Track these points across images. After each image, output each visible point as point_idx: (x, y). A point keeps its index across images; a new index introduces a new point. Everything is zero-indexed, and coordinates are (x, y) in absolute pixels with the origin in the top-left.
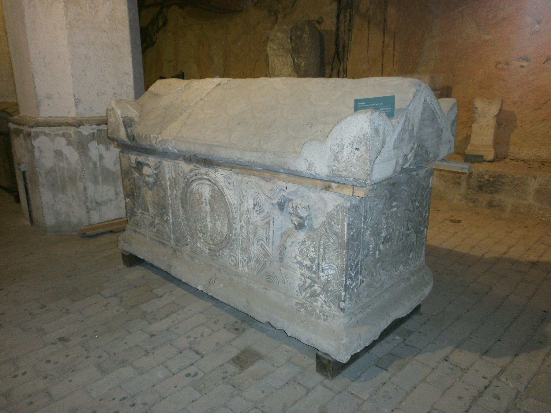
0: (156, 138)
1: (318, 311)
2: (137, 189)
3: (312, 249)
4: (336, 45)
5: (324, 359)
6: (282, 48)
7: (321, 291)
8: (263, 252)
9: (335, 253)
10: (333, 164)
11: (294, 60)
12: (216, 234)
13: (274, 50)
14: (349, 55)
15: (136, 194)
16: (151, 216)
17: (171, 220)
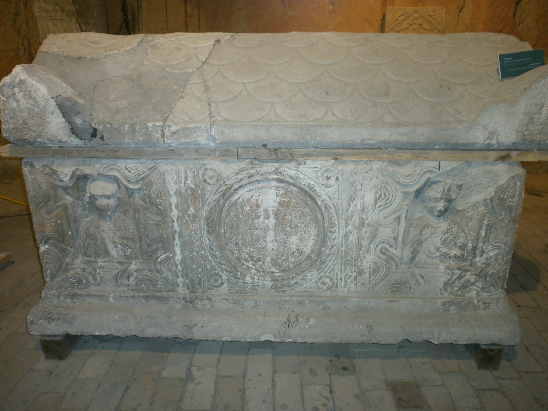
1: (476, 302)
2: (73, 223)
5: (492, 350)
6: (60, 9)
7: (475, 278)
8: (384, 257)
9: (505, 229)
12: (287, 255)
13: (47, 11)
14: (140, 24)
17: (179, 257)
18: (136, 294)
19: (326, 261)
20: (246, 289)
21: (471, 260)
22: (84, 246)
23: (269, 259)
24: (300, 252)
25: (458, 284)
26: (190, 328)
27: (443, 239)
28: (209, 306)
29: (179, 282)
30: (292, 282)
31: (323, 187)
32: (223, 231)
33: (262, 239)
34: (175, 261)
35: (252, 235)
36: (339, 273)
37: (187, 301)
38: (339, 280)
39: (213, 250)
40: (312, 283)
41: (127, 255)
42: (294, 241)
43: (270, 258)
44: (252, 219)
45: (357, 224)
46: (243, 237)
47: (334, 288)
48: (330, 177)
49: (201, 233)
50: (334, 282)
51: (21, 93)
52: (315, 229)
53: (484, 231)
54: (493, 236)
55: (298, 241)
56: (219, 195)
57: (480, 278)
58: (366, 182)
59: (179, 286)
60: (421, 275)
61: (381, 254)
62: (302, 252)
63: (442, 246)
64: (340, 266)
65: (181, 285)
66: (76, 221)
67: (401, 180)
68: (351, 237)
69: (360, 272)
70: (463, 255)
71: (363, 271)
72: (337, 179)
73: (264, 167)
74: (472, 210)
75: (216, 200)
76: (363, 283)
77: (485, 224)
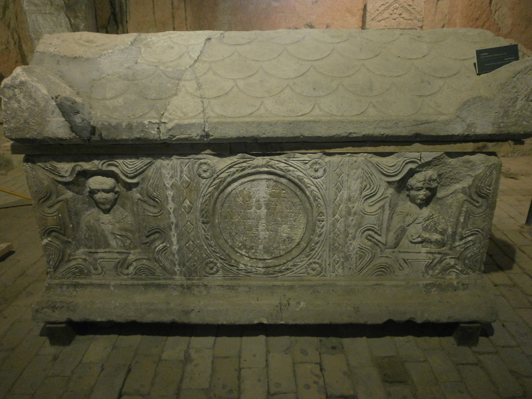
0: (157, 126)
3: (442, 221)
7: (455, 261)
11: (70, 20)
12: (278, 243)
17: (175, 247)
18: (136, 282)
20: (240, 275)
21: (451, 244)
22: (85, 238)
23: (261, 247)
25: (439, 267)
26: (187, 313)
27: (425, 225)
28: (205, 292)
30: (283, 268)
31: (311, 178)
33: (254, 228)
34: (171, 250)
36: (327, 259)
38: (327, 266)
40: (302, 269)
43: (262, 245)
47: (323, 273)
49: (196, 223)
50: (323, 267)
54: (471, 222)
56: (212, 188)
58: (352, 173)
61: (366, 241)
63: (423, 232)
64: (328, 252)
65: (178, 272)
67: (386, 170)
68: (338, 225)
69: (347, 258)
71: (350, 256)
72: (325, 171)
76: (350, 268)
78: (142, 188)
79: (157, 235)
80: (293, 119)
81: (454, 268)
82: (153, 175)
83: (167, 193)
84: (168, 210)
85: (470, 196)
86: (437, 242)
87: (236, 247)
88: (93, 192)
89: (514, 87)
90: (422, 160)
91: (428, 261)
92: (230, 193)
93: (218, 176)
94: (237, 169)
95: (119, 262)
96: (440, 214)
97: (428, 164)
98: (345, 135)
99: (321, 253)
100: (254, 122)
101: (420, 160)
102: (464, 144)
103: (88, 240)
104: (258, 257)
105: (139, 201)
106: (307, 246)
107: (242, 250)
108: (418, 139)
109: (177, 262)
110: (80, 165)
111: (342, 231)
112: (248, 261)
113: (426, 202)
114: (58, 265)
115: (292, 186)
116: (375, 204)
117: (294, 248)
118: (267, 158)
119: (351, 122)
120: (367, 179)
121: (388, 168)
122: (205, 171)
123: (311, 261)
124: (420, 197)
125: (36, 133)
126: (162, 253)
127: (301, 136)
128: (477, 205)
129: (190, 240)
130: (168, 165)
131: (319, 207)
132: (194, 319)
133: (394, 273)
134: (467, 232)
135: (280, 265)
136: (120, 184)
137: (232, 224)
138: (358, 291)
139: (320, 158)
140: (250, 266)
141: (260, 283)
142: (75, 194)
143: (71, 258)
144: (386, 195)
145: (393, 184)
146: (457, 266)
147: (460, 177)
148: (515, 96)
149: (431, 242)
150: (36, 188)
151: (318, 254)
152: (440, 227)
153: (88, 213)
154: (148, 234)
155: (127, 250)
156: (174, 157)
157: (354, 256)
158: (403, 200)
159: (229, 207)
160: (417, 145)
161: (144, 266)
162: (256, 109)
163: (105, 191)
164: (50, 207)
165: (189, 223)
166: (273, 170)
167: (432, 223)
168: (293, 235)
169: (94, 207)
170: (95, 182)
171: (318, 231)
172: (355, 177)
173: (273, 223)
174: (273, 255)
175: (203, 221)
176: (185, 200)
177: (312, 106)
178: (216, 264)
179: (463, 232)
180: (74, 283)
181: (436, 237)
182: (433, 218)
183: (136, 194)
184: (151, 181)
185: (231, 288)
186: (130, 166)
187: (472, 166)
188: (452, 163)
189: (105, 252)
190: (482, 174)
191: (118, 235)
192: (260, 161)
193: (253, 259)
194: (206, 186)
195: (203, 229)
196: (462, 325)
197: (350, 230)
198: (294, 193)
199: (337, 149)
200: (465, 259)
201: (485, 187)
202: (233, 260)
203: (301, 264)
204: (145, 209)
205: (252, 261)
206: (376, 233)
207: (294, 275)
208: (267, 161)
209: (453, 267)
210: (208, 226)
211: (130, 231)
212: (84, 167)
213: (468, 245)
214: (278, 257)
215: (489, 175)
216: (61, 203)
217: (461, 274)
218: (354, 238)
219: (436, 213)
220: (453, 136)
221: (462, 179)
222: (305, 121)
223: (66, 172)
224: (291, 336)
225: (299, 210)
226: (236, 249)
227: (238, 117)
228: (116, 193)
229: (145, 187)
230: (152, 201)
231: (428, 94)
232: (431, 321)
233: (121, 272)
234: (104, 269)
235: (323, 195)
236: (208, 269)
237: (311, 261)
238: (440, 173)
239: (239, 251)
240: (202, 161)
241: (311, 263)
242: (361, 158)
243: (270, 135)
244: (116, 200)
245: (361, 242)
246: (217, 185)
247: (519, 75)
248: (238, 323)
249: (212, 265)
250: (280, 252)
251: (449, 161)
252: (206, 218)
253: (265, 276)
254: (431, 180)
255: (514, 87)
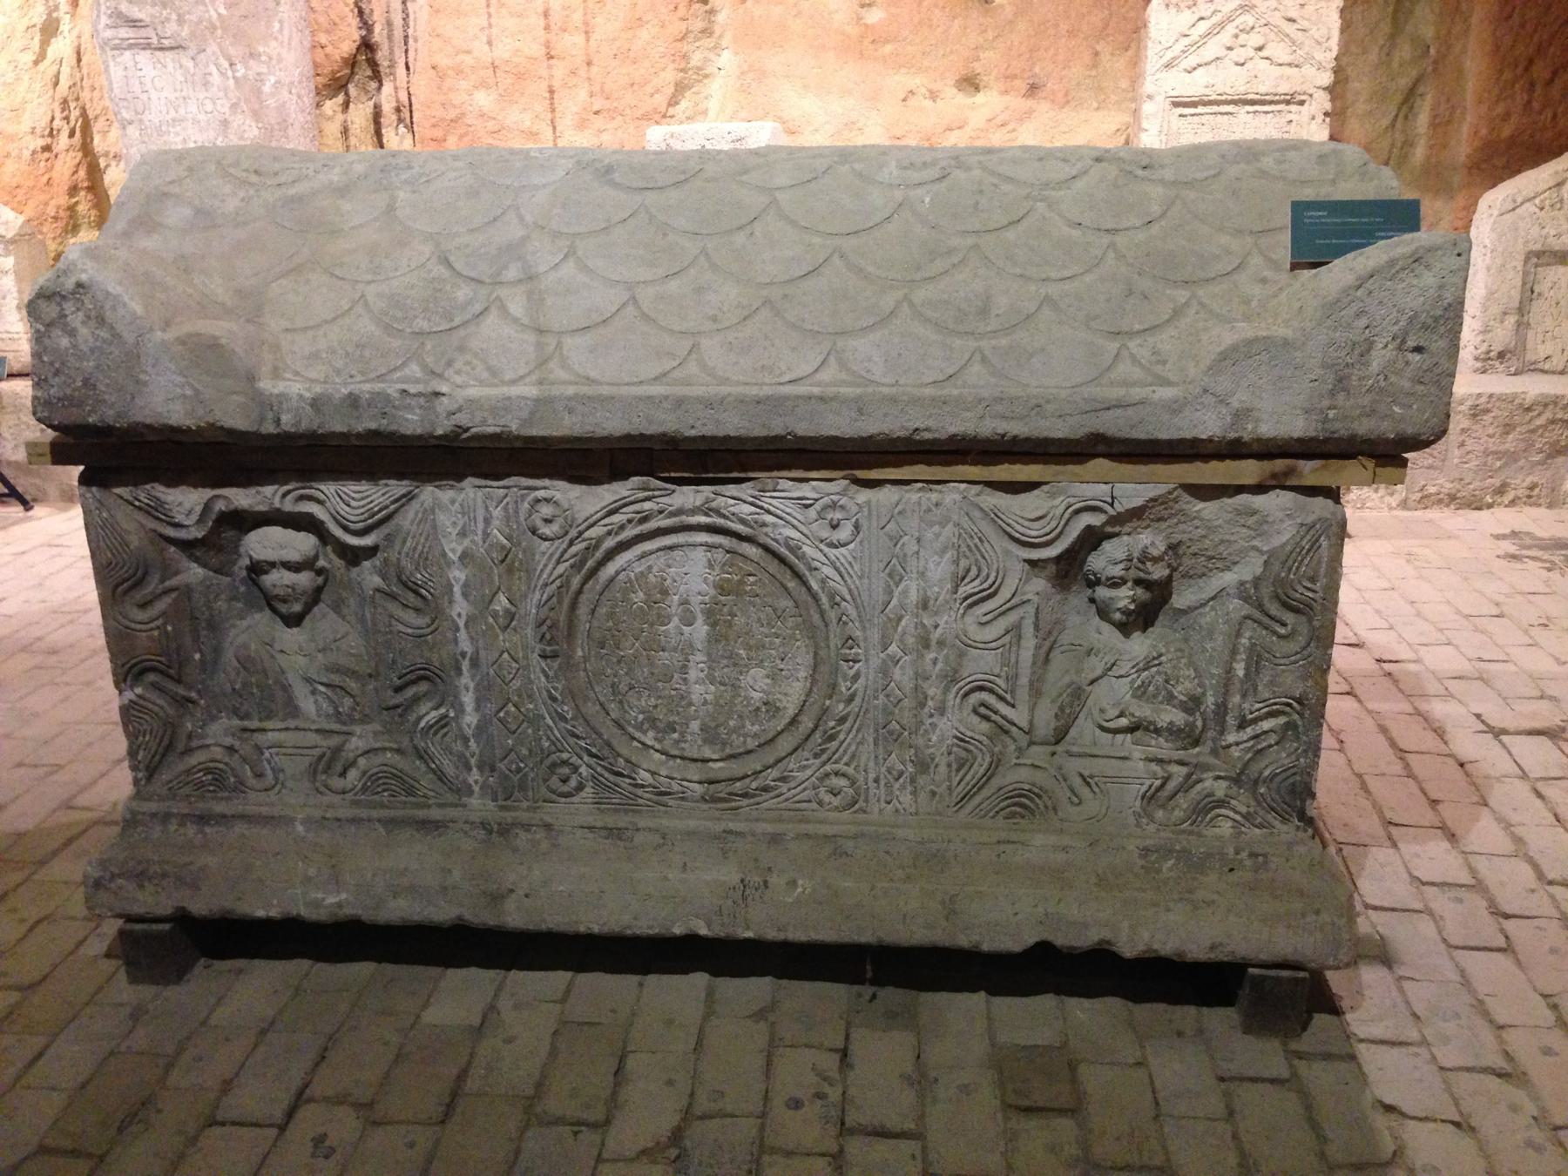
2: (205, 632)
4: (361, 13)
6: (174, 17)
10: (1326, 403)
12: (740, 717)
15: (197, 656)
16: (317, 731)
17: (470, 719)
18: (363, 813)
19: (839, 732)
20: (640, 801)
21: (1214, 740)
22: (234, 689)
23: (695, 726)
24: (771, 707)
25: (1183, 802)
26: (496, 898)
27: (1139, 682)
28: (545, 845)
29: (471, 780)
30: (754, 785)
31: (822, 546)
32: (580, 653)
33: (676, 676)
34: (460, 729)
35: (652, 665)
36: (871, 764)
37: (491, 832)
38: (871, 783)
39: (554, 699)
40: (805, 790)
41: (340, 713)
42: (756, 682)
43: (698, 722)
44: (652, 625)
45: (911, 641)
46: (630, 669)
47: (861, 804)
48: (839, 520)
49: (526, 657)
50: (859, 787)
51: (80, 314)
52: (808, 653)
53: (1242, 665)
54: (1265, 677)
55: (768, 681)
56: (567, 564)
57: (1240, 788)
58: (929, 535)
59: (471, 793)
60: (1081, 775)
61: (976, 719)
62: (778, 709)
63: (1134, 700)
64: (872, 746)
65: (476, 789)
66: (213, 626)
67: (1019, 530)
68: (897, 673)
69: (923, 765)
70: (1192, 726)
71: (933, 759)
72: (857, 527)
73: (675, 494)
74: (1213, 608)
75: (561, 576)
76: (933, 793)
77: (1244, 645)
78: (386, 560)
79: (423, 687)
80: (767, 391)
81: (1225, 808)
82: (415, 527)
83: (451, 576)
84: (453, 621)
85: (1260, 607)
86: (1173, 732)
87: (630, 724)
88: (257, 569)
89: (1359, 314)
90: (1116, 504)
91: (1148, 782)
92: (612, 580)
93: (581, 533)
94: (630, 516)
95: (323, 755)
96: (1179, 654)
97: (1136, 514)
98: (902, 434)
99: (853, 747)
100: (666, 398)
101: (1112, 505)
102: (1229, 464)
103: (241, 696)
104: (686, 754)
105: (378, 595)
106: (816, 727)
107: (644, 733)
108: (1101, 448)
109: (473, 761)
110: (226, 498)
111: (907, 690)
112: (663, 763)
113: (1142, 618)
114: (160, 762)
115: (773, 566)
116: (995, 618)
117: (783, 731)
118: (707, 490)
119: (916, 401)
120: (970, 550)
121: (1026, 523)
122: (548, 521)
123: (828, 768)
124: (1121, 604)
125: (111, 412)
126: (436, 733)
127: (789, 434)
128: (1282, 631)
129: (509, 700)
130: (453, 502)
131: (845, 623)
132: (514, 916)
133: (1056, 814)
134: (1258, 706)
135: (746, 776)
136: (329, 548)
137: (619, 662)
138: (956, 856)
139: (843, 493)
140: (667, 777)
141: (692, 824)
142: (211, 573)
143: (195, 743)
144: (1025, 598)
145: (1045, 568)
146: (1233, 802)
147: (1230, 554)
148: (1364, 337)
149: (1157, 731)
150: (109, 555)
151: (845, 752)
152: (1180, 689)
153: (245, 623)
154: (398, 682)
155: (344, 724)
156: (470, 481)
157: (943, 761)
158: (1078, 613)
159: (611, 615)
160: (1100, 465)
161: (385, 768)
162: (675, 364)
163: (288, 566)
164: (143, 606)
165: (506, 655)
166: (720, 521)
167: (1160, 679)
168: (779, 696)
169: (261, 610)
170: (266, 543)
171: (843, 687)
172: (938, 545)
173: (725, 662)
174: (728, 751)
175: (544, 650)
176: (496, 593)
177: (820, 359)
178: (576, 769)
179: (1246, 705)
180: (197, 813)
181: (1171, 716)
182: (1159, 664)
183: (369, 576)
184: (408, 544)
185: (613, 833)
186: (353, 503)
187: (1262, 525)
188: (1206, 514)
189: (287, 729)
190: (1289, 548)
191: (322, 684)
192: (687, 496)
193: (674, 757)
194: (550, 558)
195: (543, 671)
196: (1251, 970)
197: (931, 686)
198: (778, 585)
199: (887, 470)
200: (1256, 782)
201: (1300, 583)
202: (621, 760)
203: (801, 776)
204: (391, 616)
205: (671, 763)
206: (1002, 698)
207: (783, 805)
208: (707, 498)
209: (1221, 803)
210: (556, 665)
211: (352, 673)
212: (236, 503)
213: (1264, 744)
214: (740, 754)
215: (1309, 550)
216: (174, 595)
217: (1247, 825)
218: (941, 710)
219: (1168, 651)
220: (1195, 442)
221: (1237, 559)
222: (798, 397)
223: (190, 512)
224: (781, 978)
225: (791, 628)
226: (631, 730)
227: (627, 384)
228: (319, 572)
229: (393, 557)
230: (411, 596)
231: (1137, 327)
232: (1163, 953)
233: (326, 786)
234: (281, 776)
235: (856, 593)
236: (554, 782)
237: (828, 768)
238: (1174, 541)
239: (638, 735)
240: (541, 494)
241: (827, 775)
242: (951, 495)
243: (709, 430)
244: (319, 590)
245: (960, 721)
246: (577, 558)
247: (1371, 281)
248: (629, 932)
249: (566, 770)
250: (745, 742)
251: (1196, 508)
252: (549, 644)
253: (705, 806)
254: (1145, 557)
255: (1359, 314)
